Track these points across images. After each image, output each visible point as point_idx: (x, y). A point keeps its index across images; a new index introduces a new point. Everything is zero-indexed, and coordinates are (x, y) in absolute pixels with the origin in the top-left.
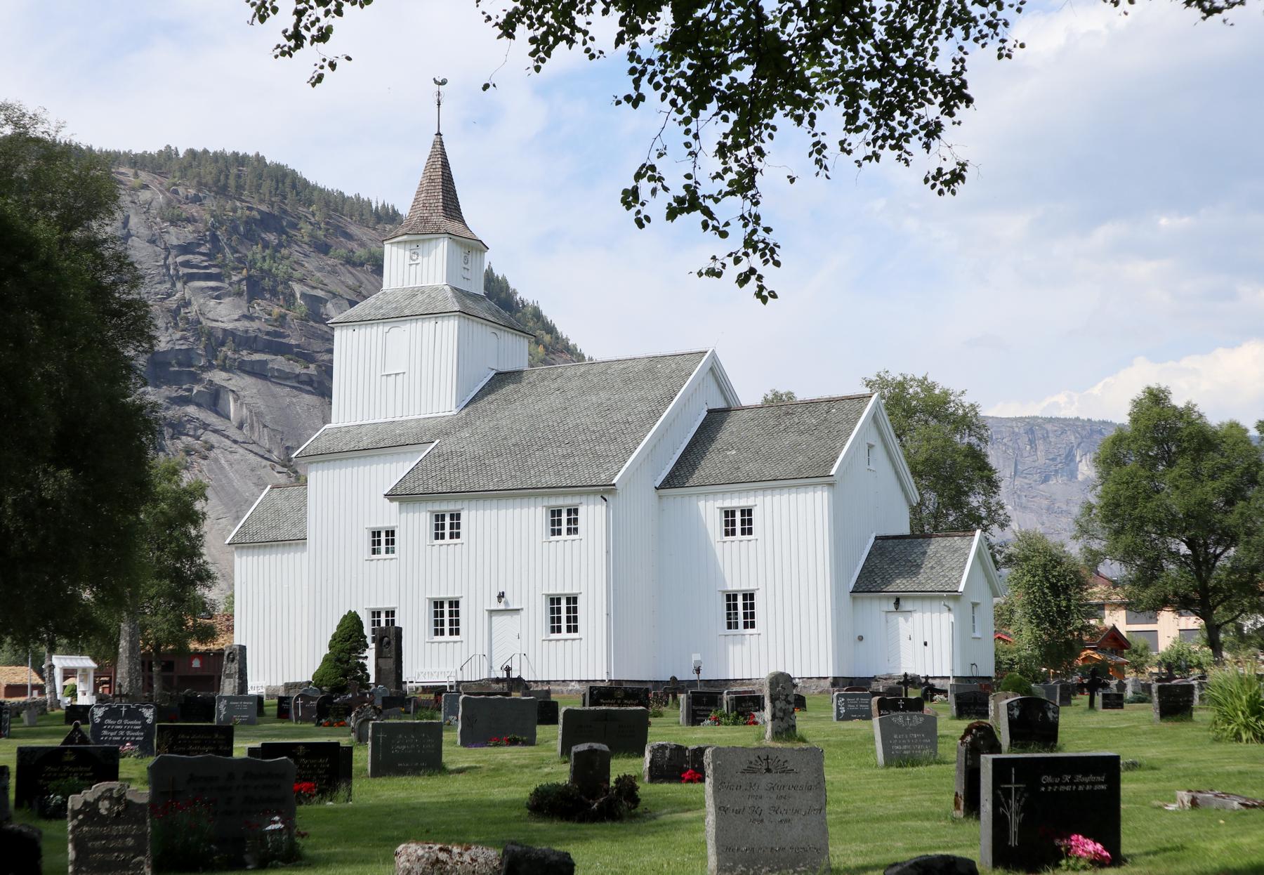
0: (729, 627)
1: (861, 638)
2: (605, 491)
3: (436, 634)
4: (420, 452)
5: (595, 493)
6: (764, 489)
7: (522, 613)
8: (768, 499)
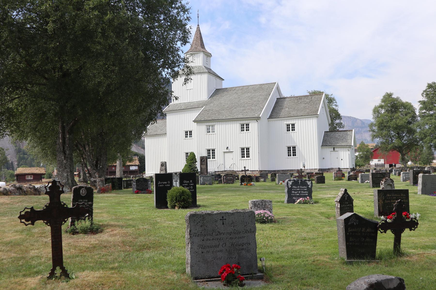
0: (289, 156)
1: (324, 158)
2: (257, 119)
3: (242, 157)
4: (200, 110)
5: (254, 120)
6: (298, 118)
7: (234, 153)
8: (302, 121)
